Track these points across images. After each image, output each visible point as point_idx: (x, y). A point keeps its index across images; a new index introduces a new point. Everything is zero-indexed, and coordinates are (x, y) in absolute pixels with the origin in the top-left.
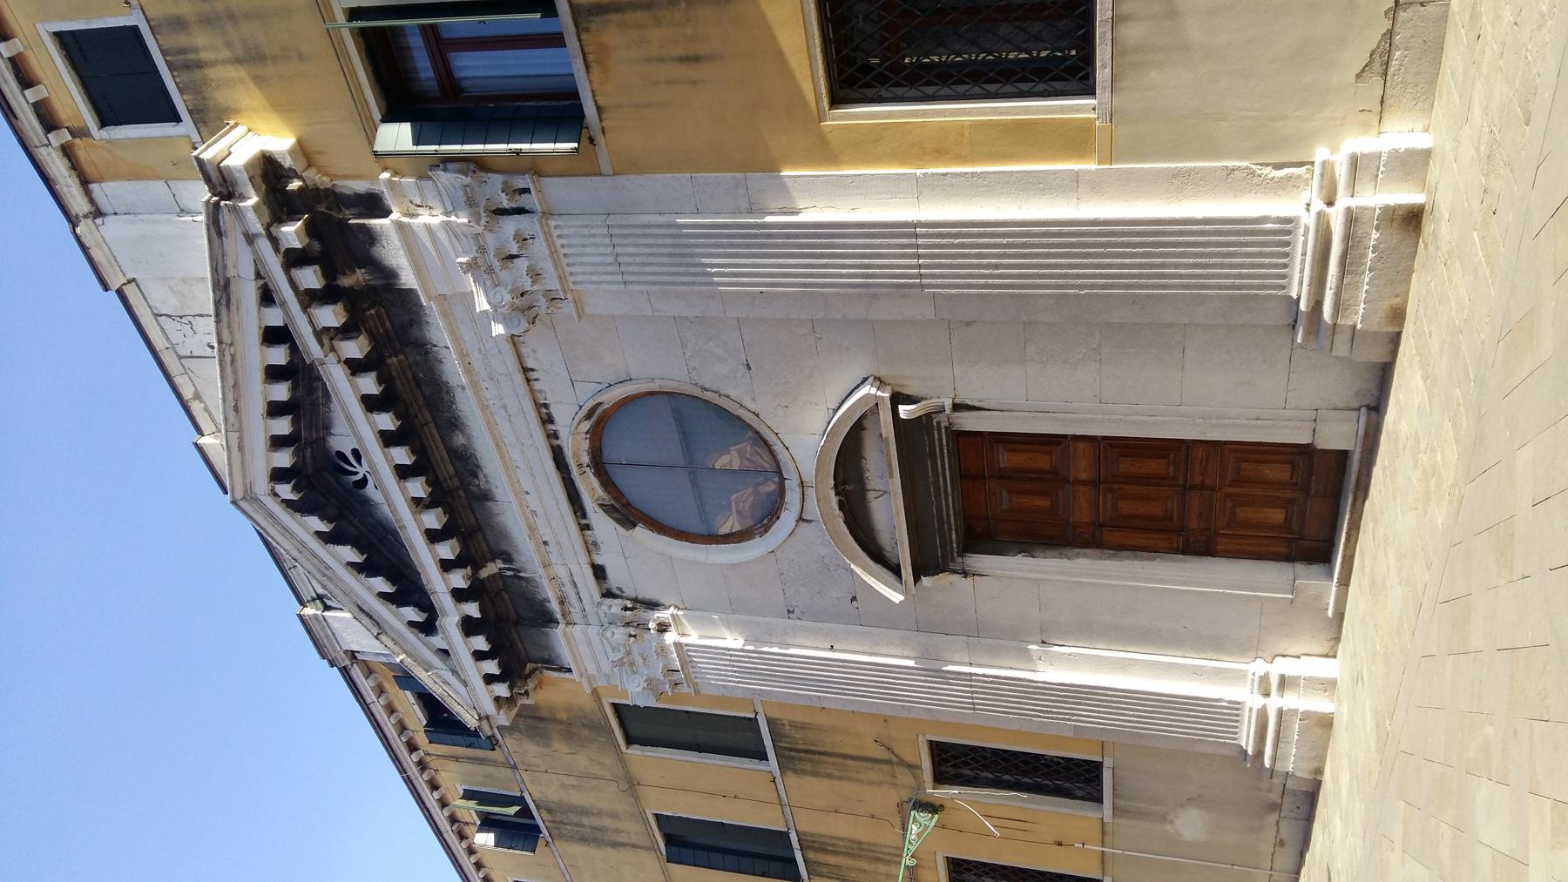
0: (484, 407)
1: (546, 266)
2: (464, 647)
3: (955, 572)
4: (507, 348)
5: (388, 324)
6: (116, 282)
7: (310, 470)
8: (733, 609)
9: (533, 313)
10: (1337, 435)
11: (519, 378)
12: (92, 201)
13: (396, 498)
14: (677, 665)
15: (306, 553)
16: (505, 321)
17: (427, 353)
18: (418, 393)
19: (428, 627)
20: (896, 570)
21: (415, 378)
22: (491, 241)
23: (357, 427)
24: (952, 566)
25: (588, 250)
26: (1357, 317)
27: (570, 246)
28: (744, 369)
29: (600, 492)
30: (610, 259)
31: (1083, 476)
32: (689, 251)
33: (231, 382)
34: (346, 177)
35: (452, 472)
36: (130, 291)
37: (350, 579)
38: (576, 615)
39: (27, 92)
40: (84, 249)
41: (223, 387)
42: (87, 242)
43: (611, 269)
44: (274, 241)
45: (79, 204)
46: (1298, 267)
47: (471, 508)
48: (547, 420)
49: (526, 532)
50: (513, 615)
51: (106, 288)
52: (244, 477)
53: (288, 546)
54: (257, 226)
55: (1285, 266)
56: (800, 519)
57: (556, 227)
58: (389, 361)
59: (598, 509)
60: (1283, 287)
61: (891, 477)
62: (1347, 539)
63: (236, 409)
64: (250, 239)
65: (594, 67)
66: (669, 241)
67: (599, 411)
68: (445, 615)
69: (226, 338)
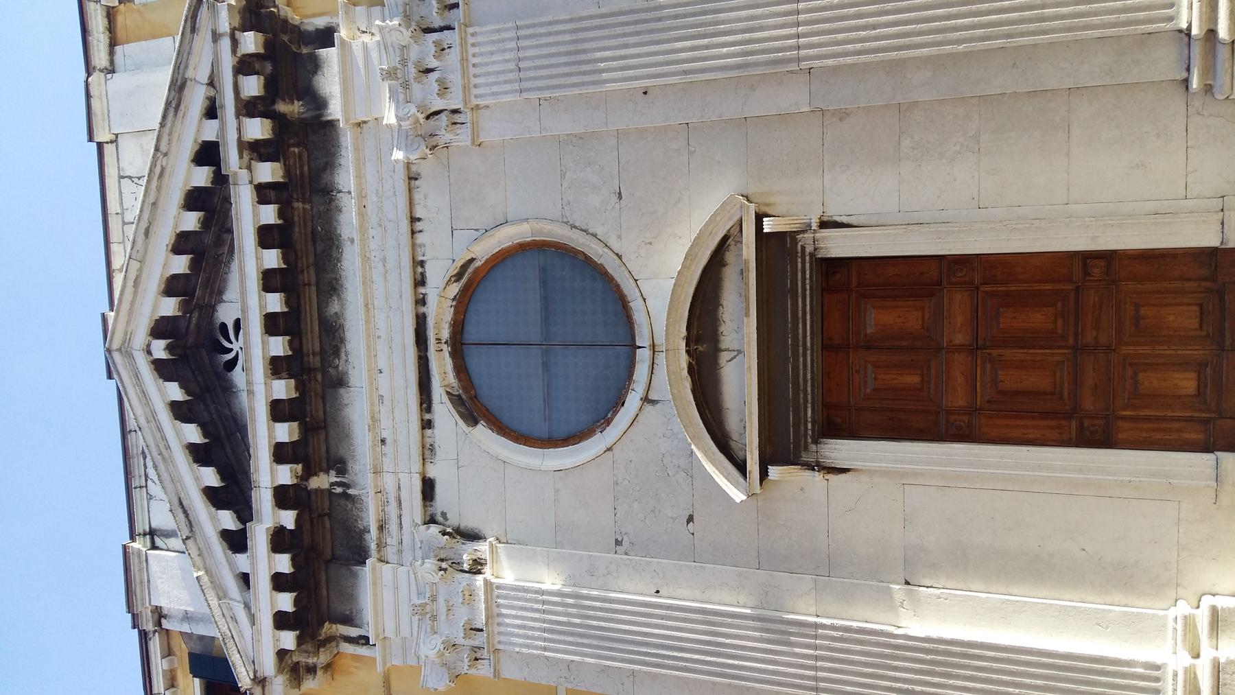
0: (366, 259)
1: (455, 80)
2: (266, 562)
3: (810, 467)
4: (401, 175)
5: (306, 168)
6: (102, 136)
7: (191, 340)
8: (557, 539)
9: (433, 141)
12: (112, 62)
13: (257, 388)
15: (153, 425)
16: (407, 148)
17: (331, 200)
18: (311, 249)
19: (236, 542)
20: (741, 467)
21: (313, 233)
22: (414, 55)
23: (246, 300)
24: (805, 457)
25: (494, 58)
27: (481, 54)
28: (615, 198)
29: (451, 378)
30: (512, 66)
31: (959, 339)
32: (589, 56)
33: (151, 199)
34: (314, 16)
35: (317, 349)
36: (109, 150)
37: (182, 460)
38: (390, 553)
40: (88, 96)
41: (144, 201)
42: (94, 91)
43: (510, 76)
44: (235, 43)
45: (100, 58)
47: (323, 398)
48: (420, 282)
49: (368, 420)
50: (328, 551)
51: (91, 139)
52: (128, 323)
53: (139, 411)
54: (224, 25)
56: (646, 400)
57: (472, 35)
58: (296, 205)
59: (445, 399)
61: (747, 315)
63: (147, 233)
64: (216, 37)
66: (567, 37)
67: (470, 270)
68: (260, 521)
69: (163, 148)
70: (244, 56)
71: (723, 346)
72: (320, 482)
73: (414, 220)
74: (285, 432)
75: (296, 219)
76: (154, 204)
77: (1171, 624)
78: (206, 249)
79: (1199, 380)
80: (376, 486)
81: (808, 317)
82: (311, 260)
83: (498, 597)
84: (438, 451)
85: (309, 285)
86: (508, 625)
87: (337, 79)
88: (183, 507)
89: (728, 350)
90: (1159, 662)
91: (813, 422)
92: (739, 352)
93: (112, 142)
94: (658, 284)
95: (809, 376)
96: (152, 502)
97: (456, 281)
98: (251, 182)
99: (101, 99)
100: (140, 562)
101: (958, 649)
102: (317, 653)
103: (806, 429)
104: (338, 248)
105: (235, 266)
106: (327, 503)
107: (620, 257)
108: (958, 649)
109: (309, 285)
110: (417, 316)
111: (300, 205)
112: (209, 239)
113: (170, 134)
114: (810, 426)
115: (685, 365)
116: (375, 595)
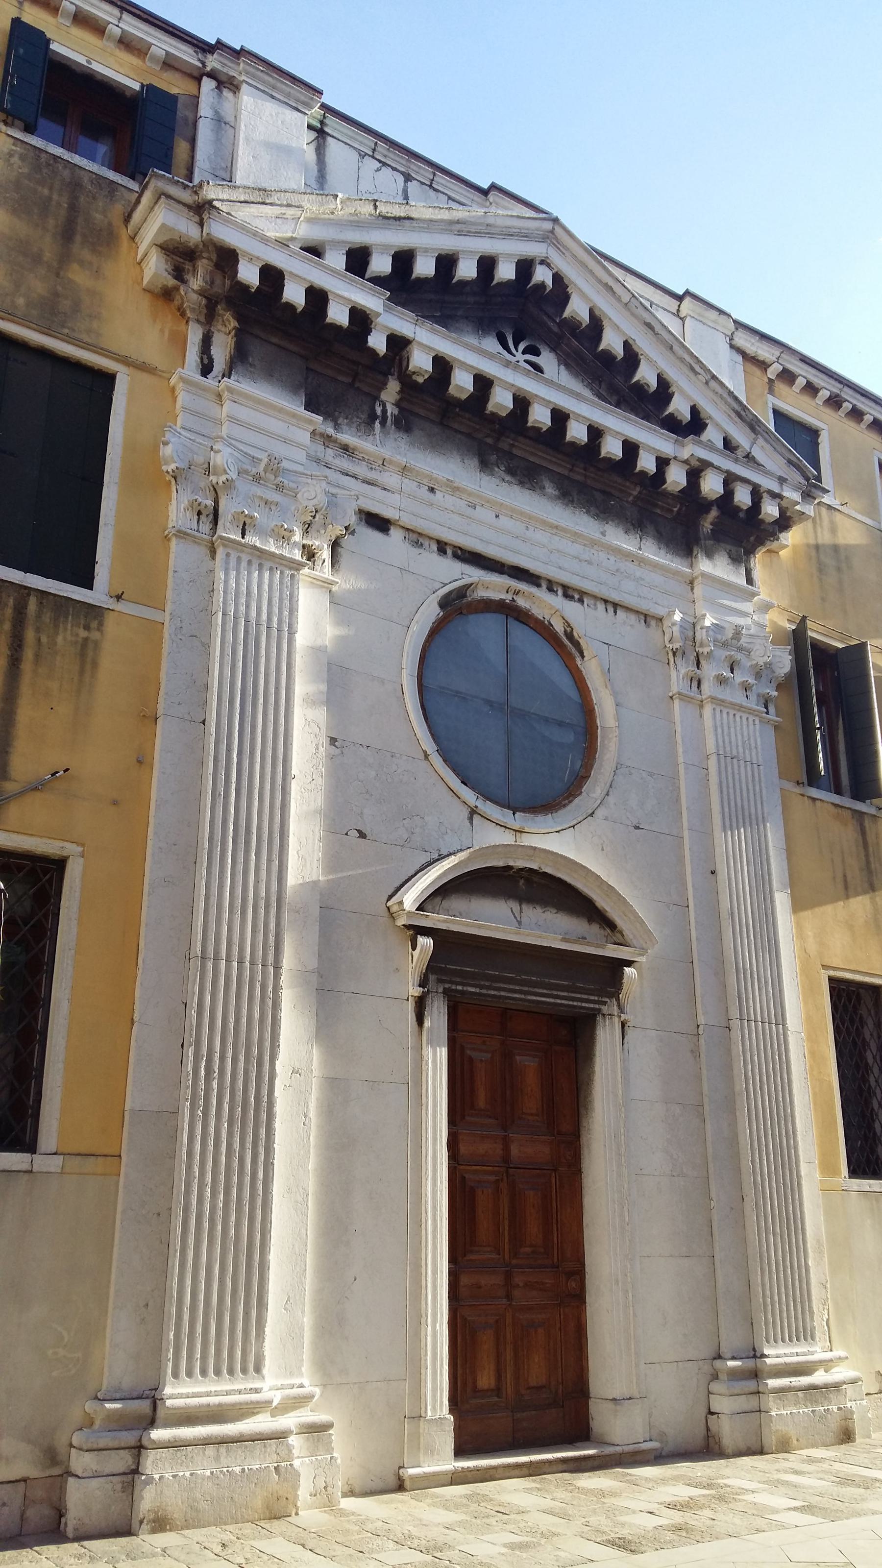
1: (726, 694)
4: (660, 611)
5: (658, 511)
10: (617, 1425)
11: (614, 596)
14: (252, 539)
23: (550, 389)
26: (777, 1410)
29: (482, 593)
30: (735, 753)
31: (515, 1150)
33: (676, 347)
35: (516, 452)
36: (673, 304)
39: (828, 394)
40: (721, 312)
46: (787, 1351)
47: (469, 436)
48: (568, 592)
52: (575, 257)
55: (783, 1341)
58: (638, 489)
59: (466, 581)
60: (768, 1342)
61: (564, 940)
62: (564, 1461)
63: (649, 326)
64: (782, 480)
65: (832, 808)
67: (577, 654)
69: (713, 384)
70: (762, 498)
71: (524, 906)
72: (391, 392)
73: (616, 606)
74: (462, 383)
75: (628, 484)
76: (671, 348)
77: (297, 1381)
78: (614, 376)
79: (487, 1390)
80: (391, 462)
81: (552, 1000)
82: (589, 482)
83: (282, 572)
84: (416, 551)
85: (571, 470)
86: (249, 573)
87: (725, 577)
88: (405, 218)
89: (521, 912)
90: (265, 1371)
91: (463, 993)
92: (520, 923)
93: (678, 311)
94: (559, 842)
95: (503, 994)
96: (355, 156)
97: (565, 631)
98: (675, 458)
99: (715, 322)
100: (297, 100)
101: (263, 1135)
102: (201, 293)
103: (457, 984)
104: (597, 516)
105: (587, 393)
106: (366, 389)
107: (592, 815)
108: (263, 1135)
109: (571, 470)
110: (538, 577)
111: (635, 493)
112: (619, 380)
113: (721, 396)
114: (460, 988)
115: (511, 864)
116: (281, 410)
